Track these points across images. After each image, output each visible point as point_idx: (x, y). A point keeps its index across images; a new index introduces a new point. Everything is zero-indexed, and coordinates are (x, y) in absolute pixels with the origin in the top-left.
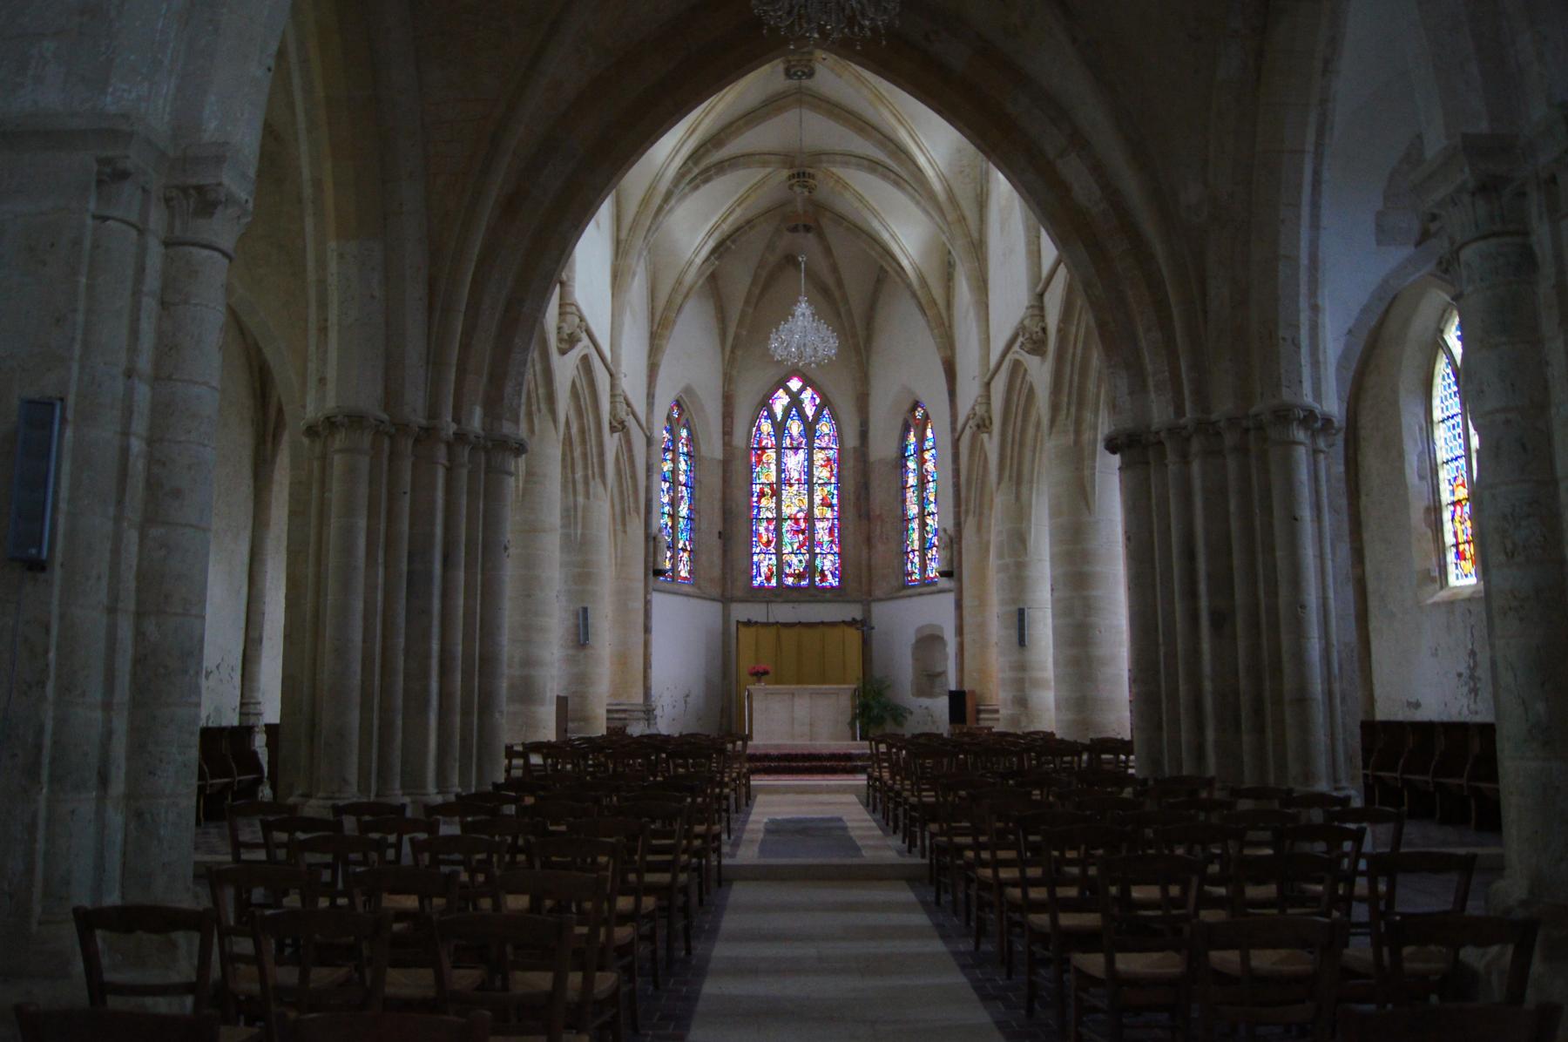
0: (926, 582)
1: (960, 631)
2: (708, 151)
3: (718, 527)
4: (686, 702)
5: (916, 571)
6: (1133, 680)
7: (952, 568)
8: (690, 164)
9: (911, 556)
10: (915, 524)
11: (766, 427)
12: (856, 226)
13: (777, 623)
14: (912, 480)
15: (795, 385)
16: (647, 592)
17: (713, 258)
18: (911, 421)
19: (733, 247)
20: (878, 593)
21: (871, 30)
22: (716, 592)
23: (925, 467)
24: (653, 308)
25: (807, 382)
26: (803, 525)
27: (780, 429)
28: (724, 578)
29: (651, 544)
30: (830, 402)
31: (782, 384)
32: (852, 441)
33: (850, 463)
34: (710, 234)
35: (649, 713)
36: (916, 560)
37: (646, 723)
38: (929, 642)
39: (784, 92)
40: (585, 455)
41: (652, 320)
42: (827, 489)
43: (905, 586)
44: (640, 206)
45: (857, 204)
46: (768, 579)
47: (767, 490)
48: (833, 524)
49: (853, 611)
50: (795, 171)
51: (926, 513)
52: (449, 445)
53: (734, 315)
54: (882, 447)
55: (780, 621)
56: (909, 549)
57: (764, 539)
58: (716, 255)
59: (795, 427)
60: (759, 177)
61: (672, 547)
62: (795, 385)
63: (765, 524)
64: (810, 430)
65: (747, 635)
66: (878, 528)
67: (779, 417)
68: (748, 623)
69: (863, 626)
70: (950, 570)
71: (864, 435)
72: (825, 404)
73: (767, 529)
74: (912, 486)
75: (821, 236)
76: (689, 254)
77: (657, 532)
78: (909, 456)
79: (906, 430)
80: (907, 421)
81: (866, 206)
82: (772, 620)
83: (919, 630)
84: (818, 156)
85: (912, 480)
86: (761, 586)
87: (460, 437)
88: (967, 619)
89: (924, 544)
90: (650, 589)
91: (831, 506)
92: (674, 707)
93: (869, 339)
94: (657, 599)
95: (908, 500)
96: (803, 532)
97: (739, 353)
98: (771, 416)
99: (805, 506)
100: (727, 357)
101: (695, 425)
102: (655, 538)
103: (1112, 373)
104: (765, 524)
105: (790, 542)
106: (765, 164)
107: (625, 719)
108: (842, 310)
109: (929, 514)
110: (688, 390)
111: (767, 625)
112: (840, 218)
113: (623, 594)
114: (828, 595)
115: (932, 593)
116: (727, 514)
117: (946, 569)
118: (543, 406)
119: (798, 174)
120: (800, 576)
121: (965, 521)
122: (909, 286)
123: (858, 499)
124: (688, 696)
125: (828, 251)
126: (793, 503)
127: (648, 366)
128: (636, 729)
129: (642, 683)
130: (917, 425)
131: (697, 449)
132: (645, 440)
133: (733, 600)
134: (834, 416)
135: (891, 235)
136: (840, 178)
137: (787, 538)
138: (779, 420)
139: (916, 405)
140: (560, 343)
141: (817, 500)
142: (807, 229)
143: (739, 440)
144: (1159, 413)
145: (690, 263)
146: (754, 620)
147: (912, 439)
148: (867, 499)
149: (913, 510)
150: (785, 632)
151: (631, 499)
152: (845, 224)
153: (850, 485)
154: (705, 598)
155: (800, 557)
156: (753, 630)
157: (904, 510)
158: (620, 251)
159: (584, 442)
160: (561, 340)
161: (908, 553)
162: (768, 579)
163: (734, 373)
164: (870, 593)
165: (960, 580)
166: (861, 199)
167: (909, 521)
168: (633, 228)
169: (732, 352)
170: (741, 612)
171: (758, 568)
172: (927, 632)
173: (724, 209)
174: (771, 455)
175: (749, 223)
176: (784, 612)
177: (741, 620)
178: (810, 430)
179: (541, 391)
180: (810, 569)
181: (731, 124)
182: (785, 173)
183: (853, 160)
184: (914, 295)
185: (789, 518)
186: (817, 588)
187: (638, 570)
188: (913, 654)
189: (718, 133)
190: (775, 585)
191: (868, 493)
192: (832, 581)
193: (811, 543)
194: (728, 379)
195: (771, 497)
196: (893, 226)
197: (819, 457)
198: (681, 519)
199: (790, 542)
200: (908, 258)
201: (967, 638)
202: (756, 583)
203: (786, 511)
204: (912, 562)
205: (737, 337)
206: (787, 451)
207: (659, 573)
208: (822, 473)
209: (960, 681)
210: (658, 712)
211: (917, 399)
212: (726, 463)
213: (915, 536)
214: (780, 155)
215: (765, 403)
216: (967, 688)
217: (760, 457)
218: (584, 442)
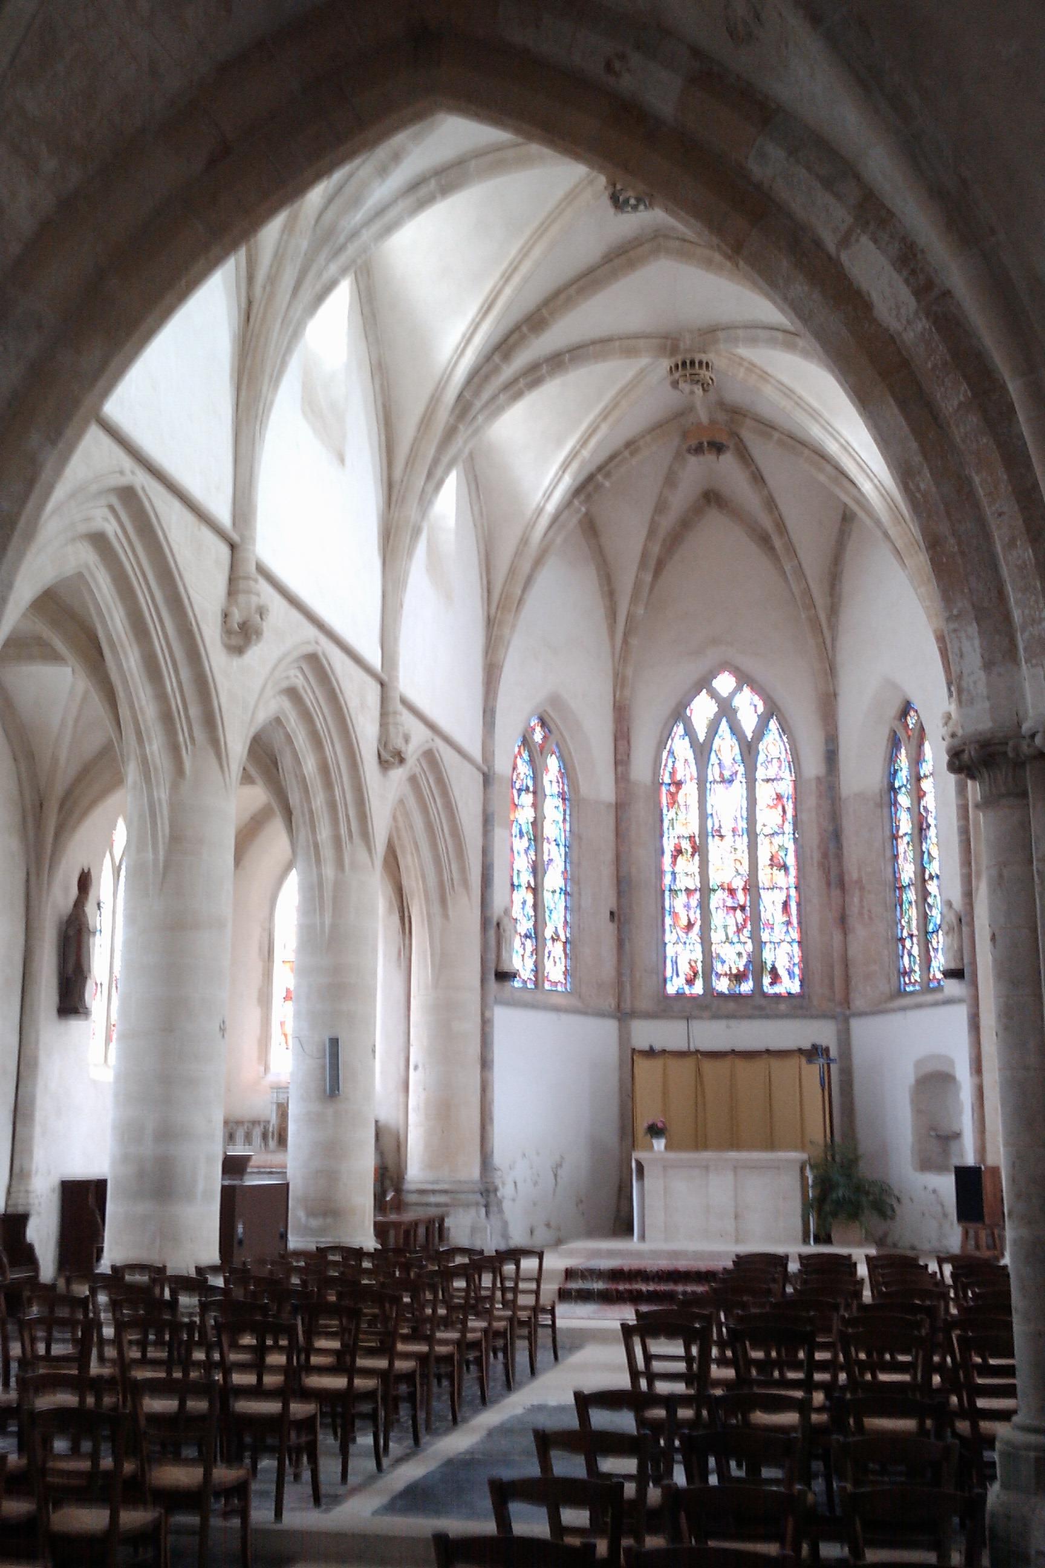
2: (523, 338)
3: (609, 901)
4: (556, 1176)
5: (917, 968)
7: (963, 965)
8: (497, 358)
9: (908, 943)
10: (911, 895)
11: (680, 746)
12: (791, 437)
13: (697, 1051)
14: (905, 825)
15: (725, 683)
17: (576, 502)
18: (901, 734)
19: (607, 484)
20: (859, 1002)
22: (609, 1003)
23: (923, 803)
24: (489, 583)
25: (744, 679)
26: (741, 898)
27: (702, 751)
28: (620, 983)
29: (492, 933)
30: (779, 710)
31: (704, 683)
32: (814, 767)
33: (811, 801)
34: (565, 467)
36: (915, 951)
37: (483, 1210)
39: (636, 239)
40: (332, 806)
41: (489, 604)
42: (778, 840)
43: (901, 993)
44: (419, 430)
45: (785, 403)
46: (690, 982)
47: (686, 845)
48: (788, 896)
49: (822, 1033)
50: (679, 359)
51: (927, 877)
53: (626, 582)
55: (701, 1049)
56: (905, 934)
57: (684, 922)
58: (582, 497)
59: (726, 747)
60: (630, 374)
62: (725, 683)
63: (682, 898)
64: (749, 750)
66: (856, 900)
67: (701, 737)
68: (651, 1053)
70: (960, 967)
71: (831, 757)
72: (772, 710)
73: (687, 906)
74: (906, 834)
75: (745, 456)
76: (537, 497)
77: (502, 914)
78: (900, 788)
79: (895, 743)
80: (895, 732)
81: (798, 404)
82: (692, 1049)
83: (918, 1064)
84: (711, 333)
85: (905, 825)
86: (680, 995)
89: (926, 925)
90: (491, 999)
91: (785, 867)
92: (536, 1184)
93: (834, 610)
94: (501, 1015)
95: (901, 856)
96: (743, 908)
97: (634, 641)
98: (690, 732)
99: (745, 869)
100: (618, 650)
101: (570, 753)
102: (498, 924)
103: (955, 631)
104: (682, 898)
105: (722, 920)
106: (630, 352)
107: (446, 1205)
108: (788, 568)
109: (931, 877)
110: (555, 700)
112: (767, 427)
114: (783, 1007)
115: (936, 1004)
116: (623, 884)
117: (953, 966)
118: (199, 733)
119: (684, 363)
120: (738, 977)
121: (977, 889)
122: (878, 523)
123: (825, 855)
124: (559, 1165)
125: (758, 478)
127: (484, 669)
129: (478, 1148)
132: (481, 778)
133: (633, 1014)
134: (784, 729)
135: (842, 445)
136: (754, 365)
137: (719, 918)
138: (701, 740)
140: (229, 638)
141: (763, 859)
142: (718, 448)
143: (640, 770)
145: (540, 511)
146: (658, 1047)
147: (903, 760)
148: (839, 856)
149: (907, 872)
150: (707, 1066)
151: (454, 867)
152: (776, 435)
153: (813, 837)
154: (584, 1013)
155: (739, 948)
156: (658, 1063)
158: (394, 498)
159: (328, 785)
160: (227, 631)
161: (902, 940)
162: (690, 982)
163: (629, 672)
164: (847, 1001)
166: (788, 392)
167: (902, 888)
168: (410, 462)
169: (625, 641)
171: (675, 963)
172: (930, 1068)
173: (584, 426)
174: (689, 792)
175: (631, 446)
177: (637, 1049)
178: (749, 750)
179: (194, 711)
180: (756, 967)
181: (557, 294)
182: (666, 364)
183: (761, 333)
184: (886, 534)
185: (722, 887)
186: (765, 995)
188: (912, 1101)
189: (538, 309)
190: (701, 992)
191: (839, 847)
192: (790, 985)
193: (754, 922)
194: (620, 681)
195: (693, 855)
196: (845, 432)
197: (765, 793)
200: (872, 481)
202: (671, 989)
203: (714, 880)
204: (910, 954)
205: (630, 617)
206: (715, 786)
208: (768, 818)
210: (506, 1191)
211: (908, 700)
212: (621, 807)
213: (913, 913)
214: (653, 337)
215: (679, 713)
217: (673, 796)
218: (328, 785)
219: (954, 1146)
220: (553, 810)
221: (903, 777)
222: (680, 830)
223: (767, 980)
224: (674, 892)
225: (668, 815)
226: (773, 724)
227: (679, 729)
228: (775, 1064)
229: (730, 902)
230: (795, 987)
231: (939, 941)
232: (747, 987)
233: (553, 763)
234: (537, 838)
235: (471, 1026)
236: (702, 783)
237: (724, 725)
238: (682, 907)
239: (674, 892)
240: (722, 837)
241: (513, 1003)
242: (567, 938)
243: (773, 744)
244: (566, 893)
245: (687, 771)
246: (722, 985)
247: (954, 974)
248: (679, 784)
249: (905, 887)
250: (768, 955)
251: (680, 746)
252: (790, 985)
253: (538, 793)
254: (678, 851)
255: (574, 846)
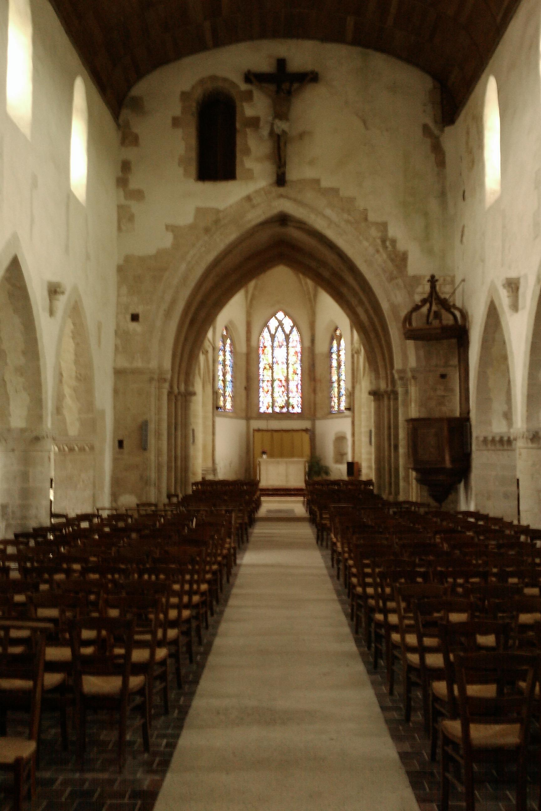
0: (339, 412)
1: (353, 435)
3: (244, 384)
6: (375, 464)
7: (350, 406)
10: (335, 385)
14: (335, 363)
15: (280, 315)
16: (213, 416)
20: (318, 415)
21: (258, 497)
22: (244, 414)
25: (286, 314)
27: (273, 337)
31: (274, 315)
32: (307, 344)
33: (306, 354)
35: (214, 470)
38: (340, 439)
43: (331, 413)
47: (268, 367)
49: (306, 424)
52: (176, 397)
54: (321, 347)
59: (280, 336)
61: (224, 396)
64: (287, 337)
65: (258, 435)
68: (259, 430)
69: (311, 432)
71: (313, 341)
79: (332, 339)
83: (336, 434)
87: (179, 393)
88: (356, 429)
104: (265, 383)
105: (279, 391)
110: (231, 322)
111: (267, 431)
113: (205, 418)
114: (295, 416)
115: (342, 417)
117: (348, 407)
120: (282, 407)
126: (280, 372)
128: (210, 477)
130: (337, 338)
131: (235, 348)
134: (299, 330)
137: (276, 389)
139: (336, 329)
144: (383, 386)
147: (335, 343)
149: (335, 378)
150: (275, 434)
153: (306, 365)
157: (331, 378)
165: (353, 412)
170: (256, 424)
174: (268, 350)
176: (275, 425)
178: (287, 337)
180: (288, 404)
187: (210, 407)
192: (298, 410)
194: (249, 315)
197: (292, 351)
198: (227, 382)
199: (279, 391)
201: (356, 438)
203: (276, 377)
207: (218, 408)
209: (353, 457)
210: (218, 470)
212: (248, 355)
213: (336, 390)
215: (266, 325)
216: (356, 460)
219: (345, 457)
220: (228, 357)
221: (335, 349)
222: (265, 362)
223: (290, 408)
224: (263, 381)
225: (262, 356)
226: (295, 329)
227: (266, 330)
228: (295, 434)
229: (280, 384)
230: (299, 410)
231: (343, 399)
232: (285, 410)
233: (229, 341)
234: (224, 365)
235: (210, 423)
236: (272, 347)
237: (280, 329)
238: (265, 386)
239: (263, 381)
240: (278, 364)
241: (220, 416)
242: (232, 395)
243: (295, 337)
244: (232, 382)
245: (268, 343)
246: (277, 410)
247: (348, 409)
248: (265, 347)
249: (334, 382)
250: (291, 401)
251: (266, 334)
252: (298, 410)
253: (224, 351)
254: (265, 368)
255: (235, 367)
